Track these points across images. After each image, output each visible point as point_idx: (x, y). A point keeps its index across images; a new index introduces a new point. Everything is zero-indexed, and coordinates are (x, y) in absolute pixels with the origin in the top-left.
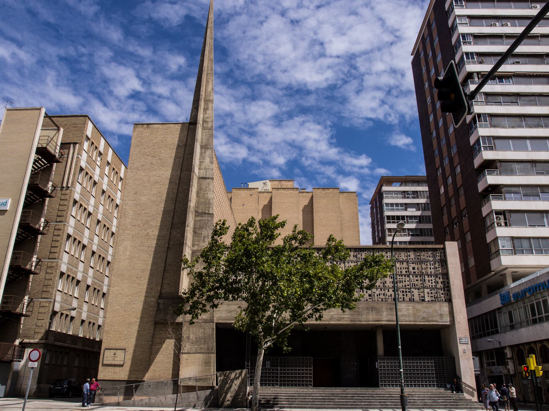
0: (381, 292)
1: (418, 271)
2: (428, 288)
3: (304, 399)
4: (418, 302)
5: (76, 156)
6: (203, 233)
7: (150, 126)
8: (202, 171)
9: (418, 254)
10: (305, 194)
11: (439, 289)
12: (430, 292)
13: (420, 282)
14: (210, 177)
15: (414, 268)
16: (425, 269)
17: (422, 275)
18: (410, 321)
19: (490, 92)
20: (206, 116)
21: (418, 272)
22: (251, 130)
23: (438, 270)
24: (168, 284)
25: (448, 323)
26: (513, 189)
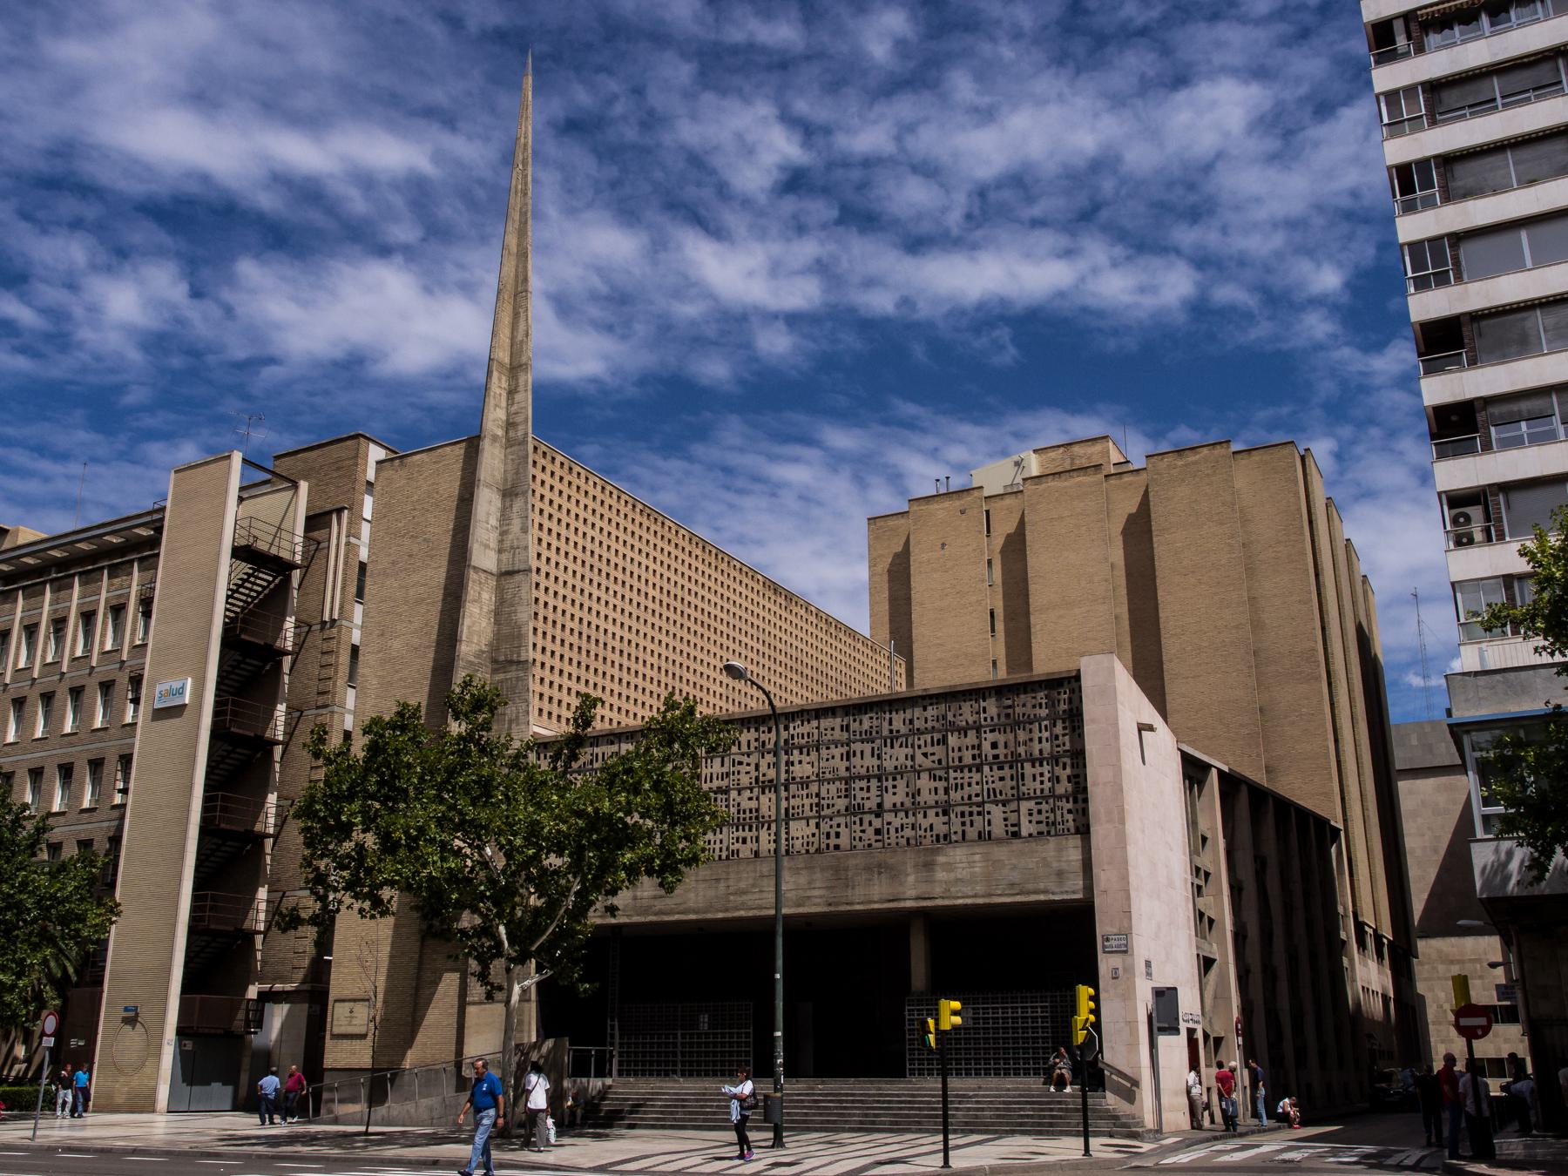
0: (905, 821)
1: (1005, 751)
2: (1030, 798)
3: (702, 1107)
4: (999, 841)
5: (343, 540)
6: (508, 712)
7: (405, 461)
8: (504, 556)
9: (1009, 702)
10: (1127, 478)
11: (1060, 797)
12: (1035, 808)
13: (1009, 783)
14: (522, 567)
15: (994, 745)
16: (1025, 744)
17: (1017, 761)
18: (975, 896)
19: (1446, 77)
20: (514, 408)
21: (1006, 756)
22: (1192, 198)
23: (1060, 742)
25: (1079, 896)
26: (1525, 406)
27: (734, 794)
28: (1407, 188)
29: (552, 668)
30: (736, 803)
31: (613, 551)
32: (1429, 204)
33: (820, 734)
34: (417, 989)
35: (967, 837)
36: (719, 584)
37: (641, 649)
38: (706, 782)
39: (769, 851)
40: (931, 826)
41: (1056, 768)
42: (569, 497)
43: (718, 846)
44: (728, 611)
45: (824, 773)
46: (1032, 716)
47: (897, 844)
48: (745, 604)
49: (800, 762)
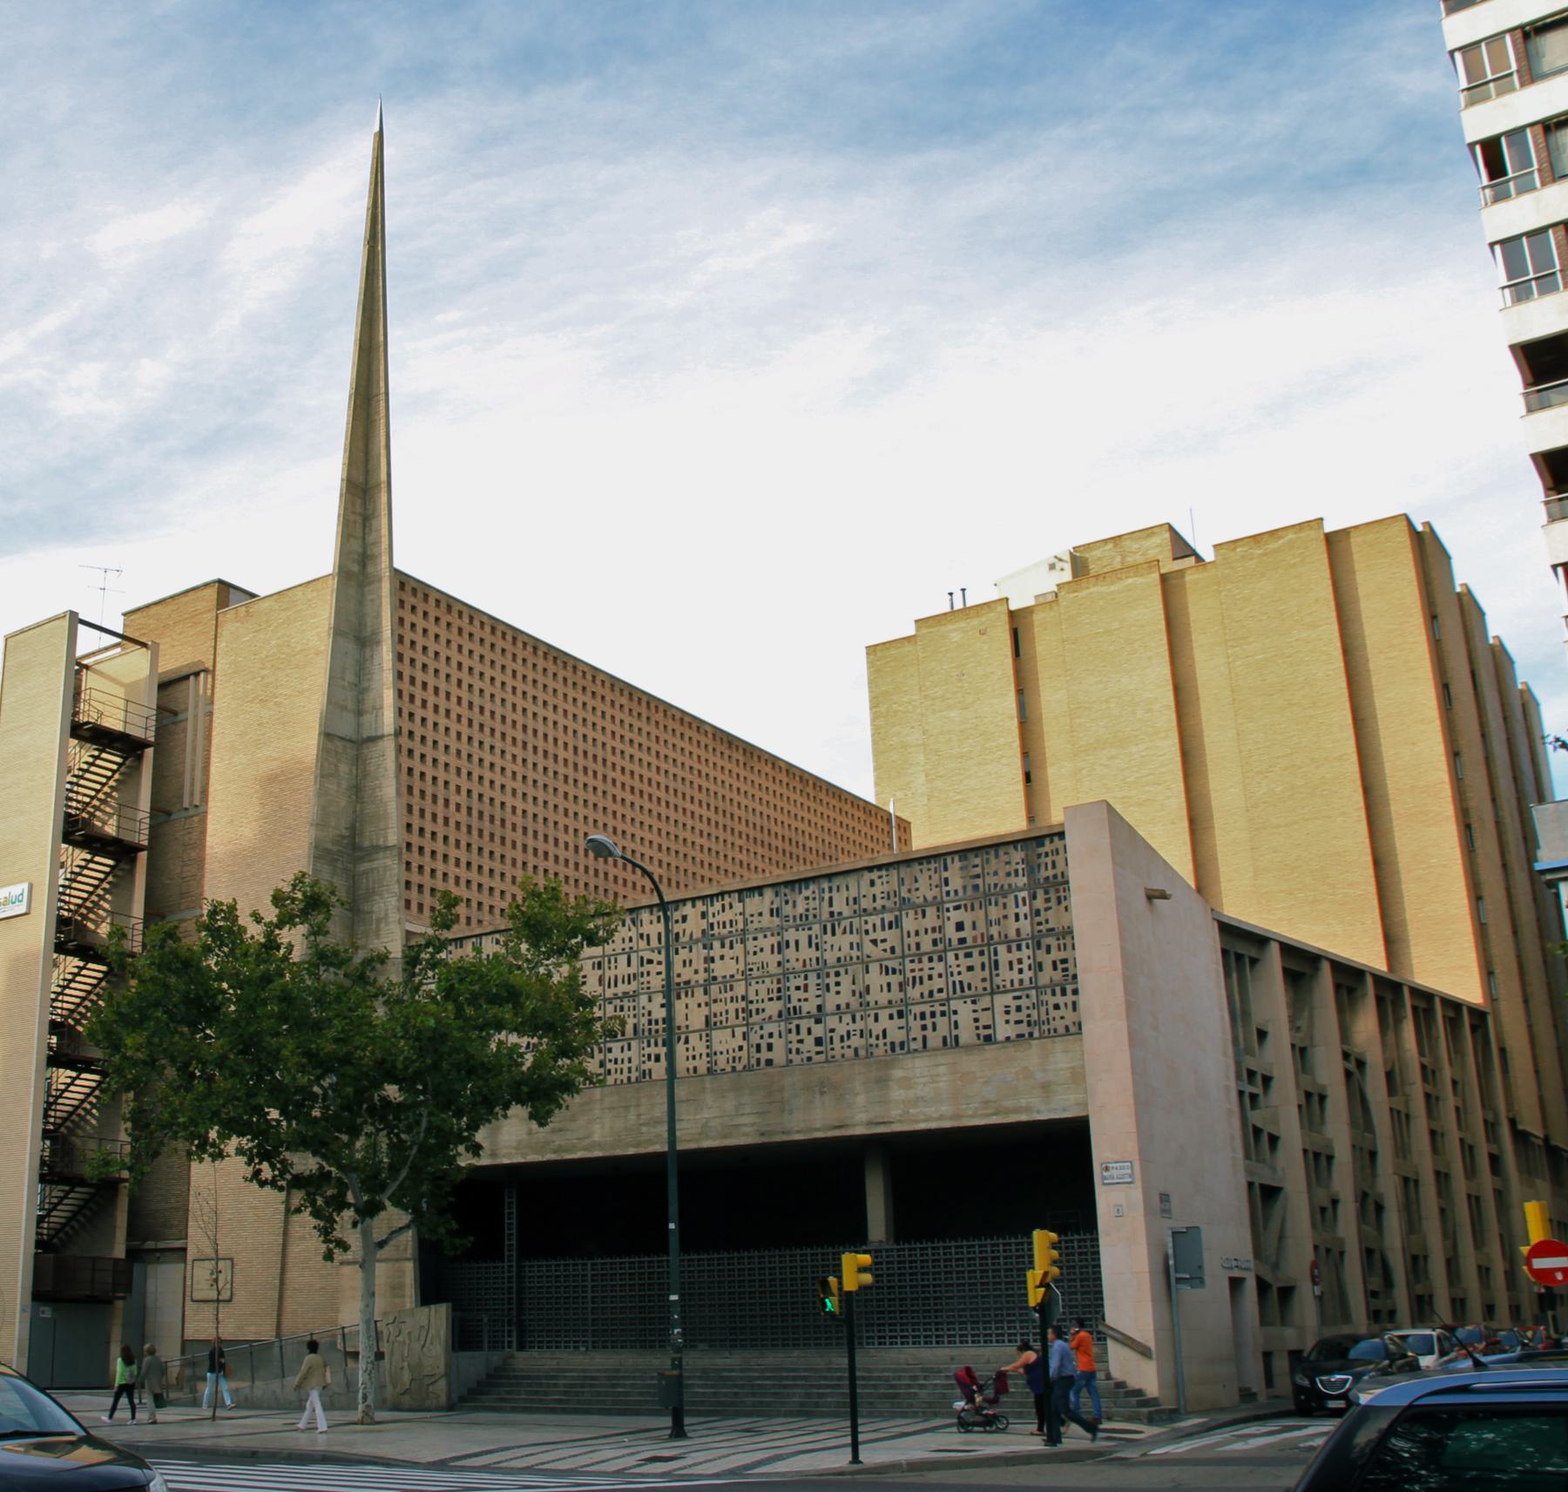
0: (851, 1027)
4: (969, 1048)
15: (960, 926)
21: (975, 939)
27: (643, 999)
28: (1495, 168)
29: (433, 853)
30: (646, 1012)
31: (509, 706)
32: (1526, 188)
33: (745, 921)
34: (285, 1246)
35: (929, 1044)
36: (654, 739)
37: (551, 824)
38: (609, 986)
39: (688, 1070)
40: (884, 1032)
41: (1038, 952)
42: (449, 642)
43: (626, 1065)
44: (666, 772)
45: (751, 970)
46: (1006, 887)
47: (843, 1056)
48: (688, 763)
49: (722, 958)
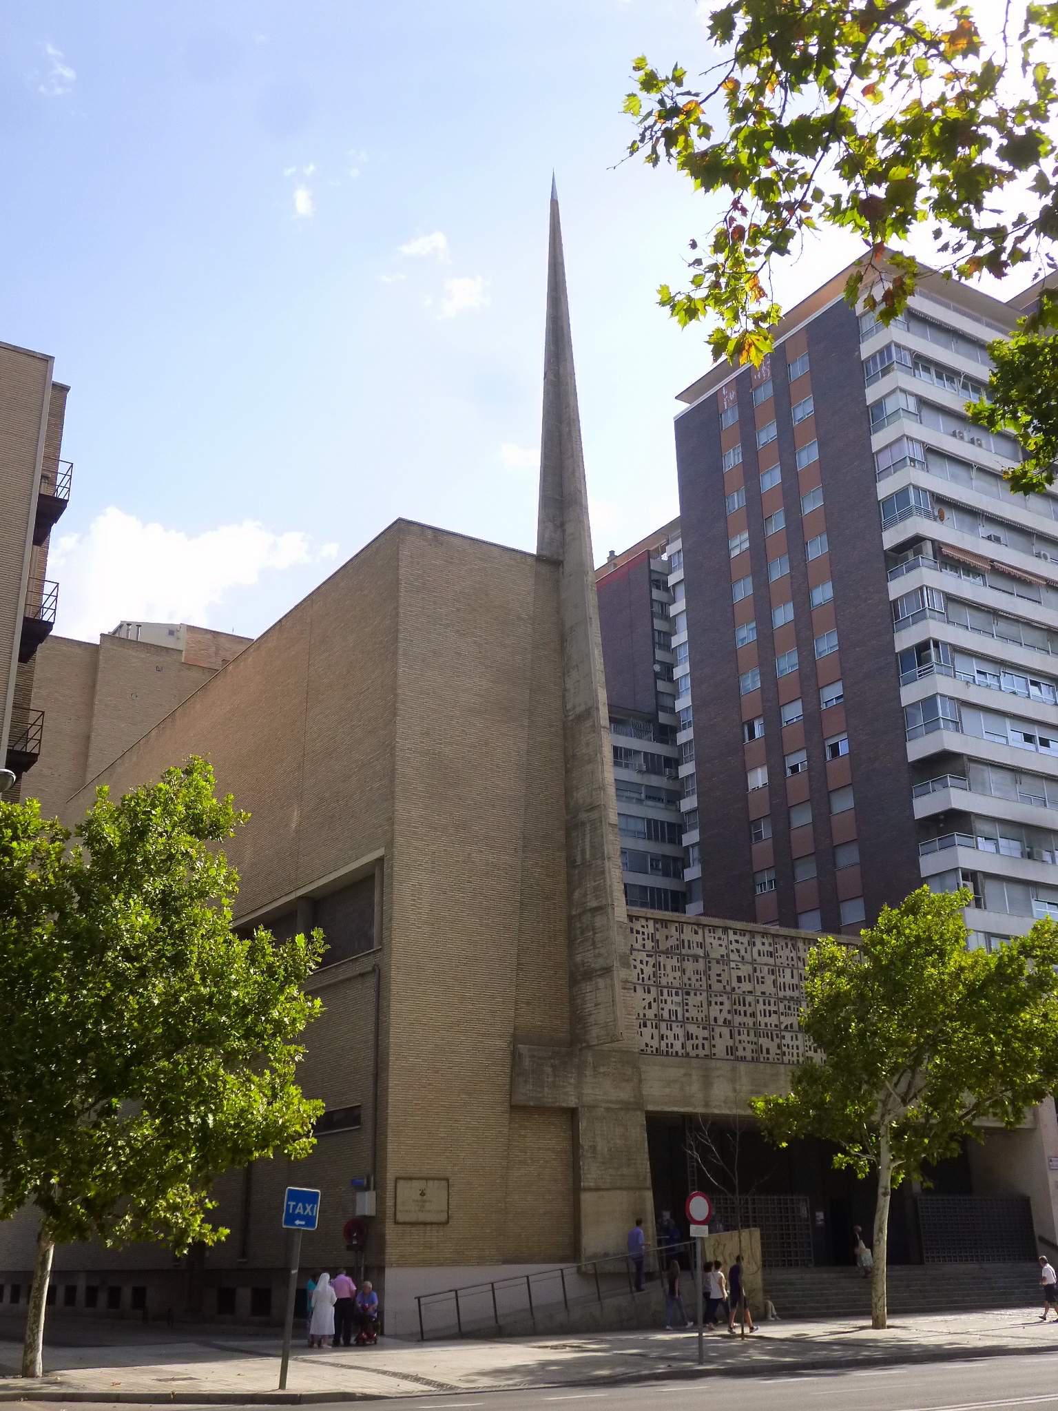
19: (1048, 535)
24: (528, 1003)
